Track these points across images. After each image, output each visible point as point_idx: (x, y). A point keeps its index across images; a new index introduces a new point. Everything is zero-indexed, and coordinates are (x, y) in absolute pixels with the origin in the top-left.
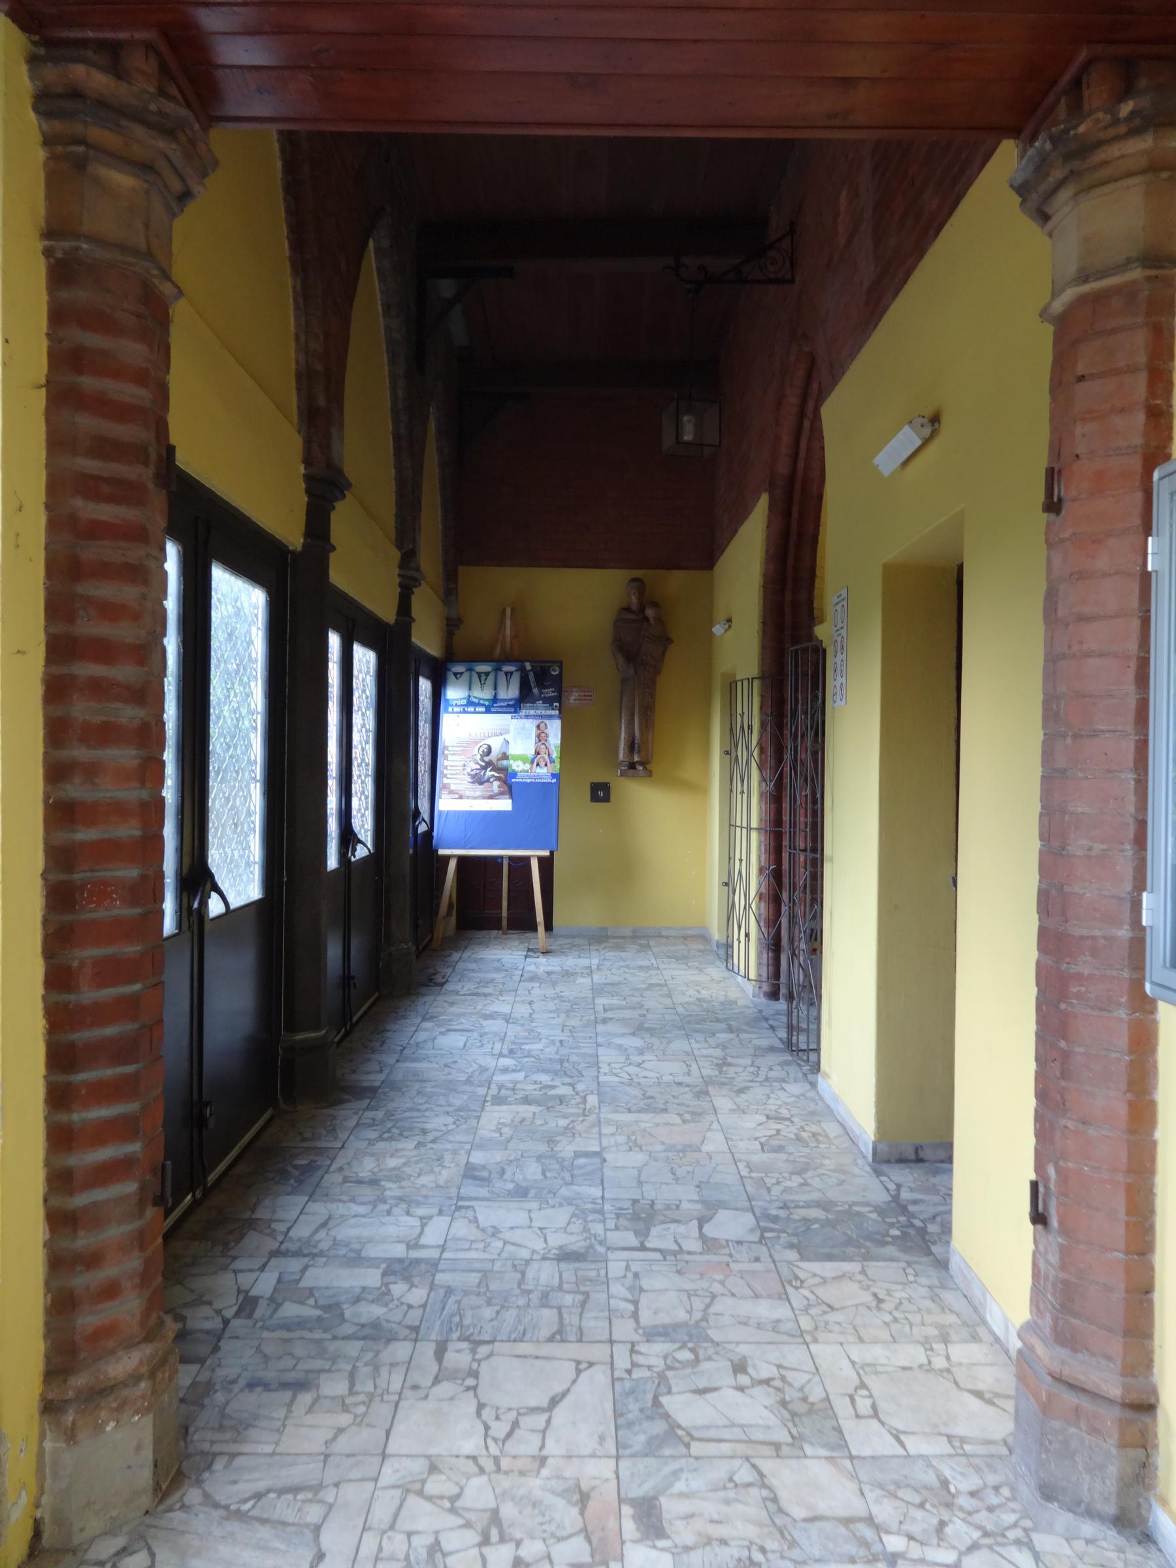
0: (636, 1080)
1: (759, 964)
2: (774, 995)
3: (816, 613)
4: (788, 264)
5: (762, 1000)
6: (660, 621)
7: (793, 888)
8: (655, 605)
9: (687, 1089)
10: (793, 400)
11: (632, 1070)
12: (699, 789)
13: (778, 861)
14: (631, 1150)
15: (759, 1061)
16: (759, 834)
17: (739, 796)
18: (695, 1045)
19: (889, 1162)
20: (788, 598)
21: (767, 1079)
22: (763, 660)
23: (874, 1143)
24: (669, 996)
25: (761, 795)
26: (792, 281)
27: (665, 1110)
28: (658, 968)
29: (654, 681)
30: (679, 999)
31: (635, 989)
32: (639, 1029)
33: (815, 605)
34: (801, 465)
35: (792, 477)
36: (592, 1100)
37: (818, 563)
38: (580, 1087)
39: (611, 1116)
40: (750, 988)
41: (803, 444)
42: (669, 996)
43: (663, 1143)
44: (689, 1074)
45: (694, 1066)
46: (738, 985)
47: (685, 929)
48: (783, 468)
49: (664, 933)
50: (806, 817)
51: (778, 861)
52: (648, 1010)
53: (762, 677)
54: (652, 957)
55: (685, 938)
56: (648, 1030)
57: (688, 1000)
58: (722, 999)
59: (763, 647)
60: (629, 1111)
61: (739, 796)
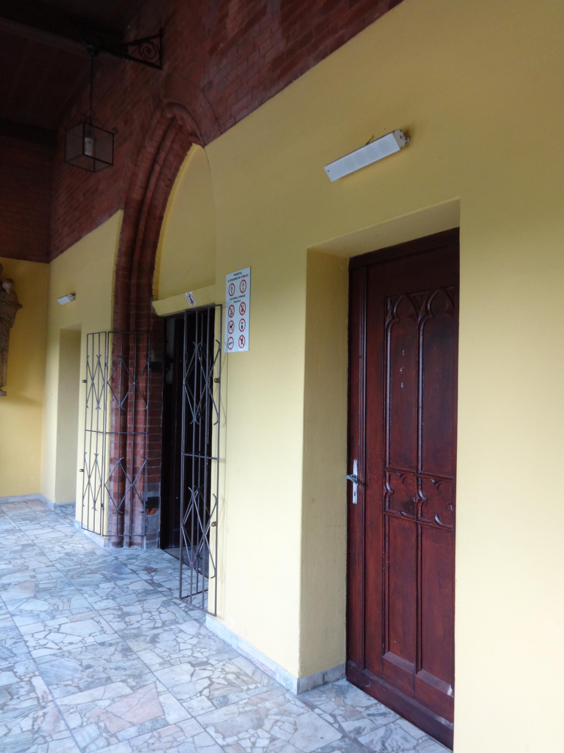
0: (65, 649)
1: (109, 524)
2: (119, 544)
3: (154, 293)
4: (158, 56)
5: (111, 548)
6: (13, 292)
7: (135, 470)
8: (10, 281)
9: (112, 649)
10: (150, 149)
11: (53, 636)
12: (38, 404)
13: (124, 454)
14: (109, 744)
15: (146, 605)
16: (110, 436)
17: (95, 411)
18: (90, 600)
19: (307, 691)
20: (134, 281)
21: (164, 623)
22: (115, 321)
23: (299, 680)
24: (42, 554)
25: (112, 411)
26: (160, 68)
27: (109, 680)
28: (20, 530)
29: (8, 332)
30: (53, 556)
31: (15, 552)
32: (38, 592)
33: (153, 288)
34: (149, 194)
35: (142, 203)
36: (38, 682)
37: (156, 260)
38: (20, 670)
39: (67, 700)
40: (101, 541)
41: (153, 181)
42: (42, 554)
43: (133, 725)
44: (103, 631)
45: (102, 621)
46: (87, 538)
47: (25, 496)
48: (136, 195)
49: (11, 500)
50: (145, 424)
51: (124, 454)
52: (34, 570)
53: (115, 331)
54: (10, 521)
55: (26, 502)
56: (45, 590)
57: (59, 556)
58: (83, 552)
59: (115, 312)
60: (81, 690)
61: (95, 411)
